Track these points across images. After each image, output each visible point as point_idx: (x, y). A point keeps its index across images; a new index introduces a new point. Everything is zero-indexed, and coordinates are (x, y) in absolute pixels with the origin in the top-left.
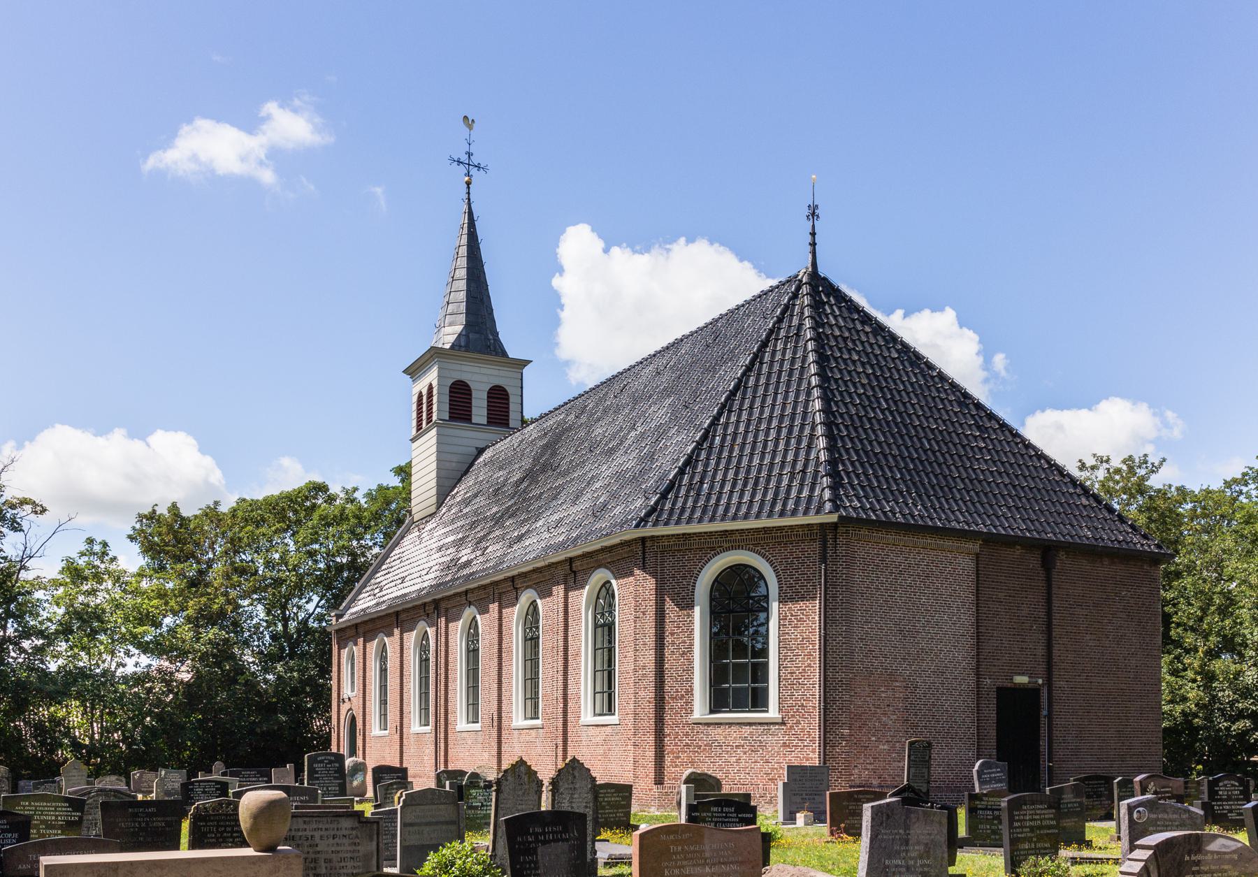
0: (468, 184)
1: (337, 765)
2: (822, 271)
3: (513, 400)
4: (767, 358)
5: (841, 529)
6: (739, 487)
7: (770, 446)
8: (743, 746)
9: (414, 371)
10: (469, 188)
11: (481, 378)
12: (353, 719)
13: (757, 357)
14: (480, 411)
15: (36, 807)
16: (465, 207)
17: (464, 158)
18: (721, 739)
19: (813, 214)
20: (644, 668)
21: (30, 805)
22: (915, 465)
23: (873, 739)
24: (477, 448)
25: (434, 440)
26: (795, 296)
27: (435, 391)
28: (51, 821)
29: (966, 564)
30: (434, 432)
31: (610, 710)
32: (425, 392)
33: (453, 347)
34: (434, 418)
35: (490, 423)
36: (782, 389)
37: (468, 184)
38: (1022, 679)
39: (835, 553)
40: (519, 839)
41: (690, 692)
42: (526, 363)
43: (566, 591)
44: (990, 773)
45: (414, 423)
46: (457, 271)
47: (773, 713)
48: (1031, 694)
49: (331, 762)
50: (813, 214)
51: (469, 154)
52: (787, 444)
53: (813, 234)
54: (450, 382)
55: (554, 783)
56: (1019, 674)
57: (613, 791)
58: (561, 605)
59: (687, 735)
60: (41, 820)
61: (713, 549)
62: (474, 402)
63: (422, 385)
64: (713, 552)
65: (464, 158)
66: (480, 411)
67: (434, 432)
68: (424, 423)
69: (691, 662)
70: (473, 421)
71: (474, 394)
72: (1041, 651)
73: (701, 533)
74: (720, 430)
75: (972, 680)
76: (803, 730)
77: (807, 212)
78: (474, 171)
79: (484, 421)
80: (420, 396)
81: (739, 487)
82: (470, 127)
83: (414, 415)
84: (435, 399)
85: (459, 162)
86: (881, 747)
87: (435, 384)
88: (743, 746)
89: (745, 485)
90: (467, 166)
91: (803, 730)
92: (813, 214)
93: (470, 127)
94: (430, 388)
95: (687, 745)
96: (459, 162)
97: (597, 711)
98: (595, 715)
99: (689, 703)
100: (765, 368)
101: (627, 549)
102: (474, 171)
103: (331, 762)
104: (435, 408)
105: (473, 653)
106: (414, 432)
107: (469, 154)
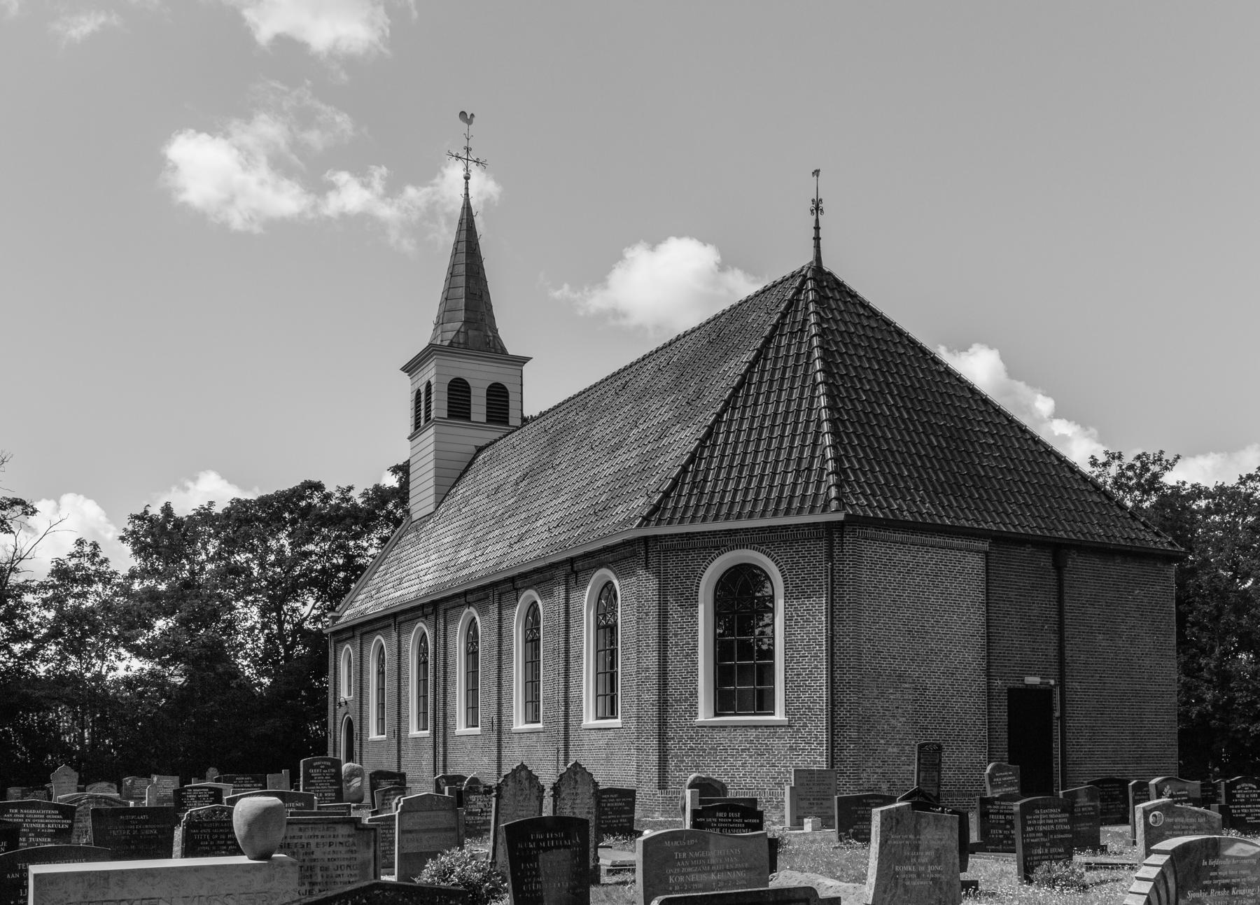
1: (333, 770)
2: (827, 266)
3: (513, 397)
5: (848, 528)
8: (749, 749)
10: (467, 183)
11: (480, 375)
12: (350, 724)
14: (479, 408)
19: (817, 208)
20: (647, 670)
21: (19, 813)
23: (882, 741)
24: (476, 447)
25: (432, 439)
26: (799, 291)
27: (433, 389)
29: (975, 563)
32: (423, 390)
34: (433, 416)
41: (694, 694)
42: (527, 359)
44: (1001, 777)
48: (1043, 695)
49: (327, 767)
50: (817, 209)
53: (817, 228)
56: (1031, 675)
59: (691, 738)
61: (717, 548)
64: (717, 552)
66: (479, 408)
67: (432, 431)
68: (422, 423)
69: (695, 663)
72: (1052, 652)
76: (810, 733)
77: (811, 206)
79: (484, 419)
82: (469, 122)
86: (890, 750)
87: (433, 381)
88: (749, 749)
90: (465, 161)
91: (810, 733)
92: (817, 209)
93: (469, 122)
94: (429, 385)
95: (692, 748)
96: (477, 162)
99: (694, 705)
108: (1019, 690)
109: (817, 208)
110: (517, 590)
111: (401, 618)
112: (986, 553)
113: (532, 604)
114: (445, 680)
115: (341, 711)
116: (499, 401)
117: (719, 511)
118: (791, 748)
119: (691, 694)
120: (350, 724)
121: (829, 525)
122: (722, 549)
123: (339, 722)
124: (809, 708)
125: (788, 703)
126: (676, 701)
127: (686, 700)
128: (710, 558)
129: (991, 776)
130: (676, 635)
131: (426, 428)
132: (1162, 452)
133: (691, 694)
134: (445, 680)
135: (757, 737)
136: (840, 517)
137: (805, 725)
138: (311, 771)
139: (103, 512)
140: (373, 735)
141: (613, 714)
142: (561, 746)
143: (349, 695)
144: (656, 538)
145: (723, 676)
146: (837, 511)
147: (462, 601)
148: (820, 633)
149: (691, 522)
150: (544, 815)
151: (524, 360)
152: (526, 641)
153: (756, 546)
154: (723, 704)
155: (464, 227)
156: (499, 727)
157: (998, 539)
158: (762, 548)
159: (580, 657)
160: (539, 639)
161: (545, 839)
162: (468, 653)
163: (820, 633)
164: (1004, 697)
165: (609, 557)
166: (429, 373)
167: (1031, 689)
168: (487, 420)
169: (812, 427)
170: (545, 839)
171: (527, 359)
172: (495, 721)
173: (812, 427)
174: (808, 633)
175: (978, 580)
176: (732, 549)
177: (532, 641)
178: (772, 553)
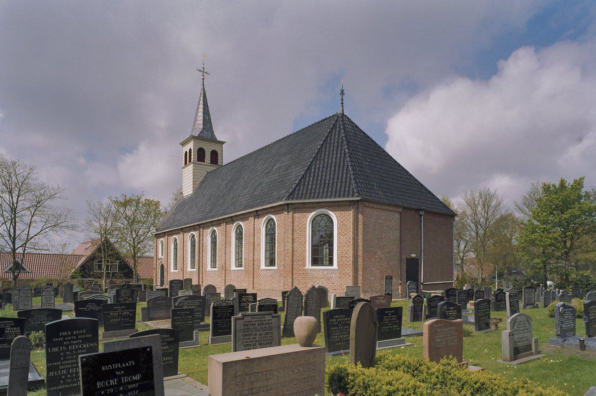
0: (203, 79)
3: (219, 155)
4: (328, 142)
5: (360, 203)
6: (322, 186)
7: (332, 172)
9: (183, 144)
11: (208, 148)
12: (162, 266)
13: (325, 140)
16: (202, 87)
17: (202, 69)
19: (342, 93)
22: (362, 181)
25: (192, 168)
26: (337, 121)
27: (192, 151)
29: (397, 216)
30: (192, 165)
32: (188, 151)
34: (192, 160)
35: (211, 163)
36: (335, 152)
37: (203, 79)
38: (414, 255)
40: (331, 320)
41: (305, 258)
42: (224, 142)
45: (184, 162)
47: (335, 266)
49: (178, 283)
50: (342, 93)
51: (204, 68)
52: (339, 172)
53: (342, 100)
55: (307, 296)
58: (253, 227)
61: (313, 208)
62: (206, 155)
63: (186, 148)
65: (202, 69)
67: (192, 165)
68: (188, 162)
69: (305, 247)
71: (206, 153)
74: (313, 167)
75: (399, 255)
77: (340, 92)
78: (205, 74)
80: (186, 152)
81: (322, 186)
83: (184, 159)
84: (192, 154)
85: (200, 71)
87: (192, 148)
89: (324, 186)
92: (342, 93)
94: (190, 150)
95: (304, 277)
96: (200, 71)
97: (237, 266)
98: (211, 268)
99: (305, 262)
100: (328, 146)
101: (281, 207)
102: (205, 74)
103: (178, 283)
104: (192, 157)
105: (214, 242)
106: (184, 165)
107: (204, 68)
108: (410, 259)
109: (342, 93)
110: (233, 221)
111: (184, 230)
112: (400, 213)
113: (239, 226)
115: (159, 262)
116: (215, 157)
117: (314, 195)
120: (162, 266)
121: (358, 201)
123: (158, 266)
124: (346, 264)
125: (338, 262)
129: (409, 285)
130: (298, 238)
131: (189, 165)
133: (304, 259)
135: (327, 274)
136: (359, 198)
139: (513, 54)
140: (172, 270)
143: (162, 255)
144: (291, 204)
145: (316, 250)
146: (357, 196)
147: (210, 224)
148: (350, 238)
149: (313, 198)
150: (474, 321)
151: (223, 143)
152: (236, 239)
154: (315, 261)
155: (202, 95)
156: (225, 269)
157: (404, 208)
159: (259, 244)
160: (216, 242)
161: (339, 318)
162: (191, 246)
164: (405, 261)
165: (273, 210)
166: (191, 145)
167: (413, 259)
169: (346, 167)
170: (339, 318)
171: (224, 142)
172: (224, 267)
173: (346, 167)
177: (214, 242)
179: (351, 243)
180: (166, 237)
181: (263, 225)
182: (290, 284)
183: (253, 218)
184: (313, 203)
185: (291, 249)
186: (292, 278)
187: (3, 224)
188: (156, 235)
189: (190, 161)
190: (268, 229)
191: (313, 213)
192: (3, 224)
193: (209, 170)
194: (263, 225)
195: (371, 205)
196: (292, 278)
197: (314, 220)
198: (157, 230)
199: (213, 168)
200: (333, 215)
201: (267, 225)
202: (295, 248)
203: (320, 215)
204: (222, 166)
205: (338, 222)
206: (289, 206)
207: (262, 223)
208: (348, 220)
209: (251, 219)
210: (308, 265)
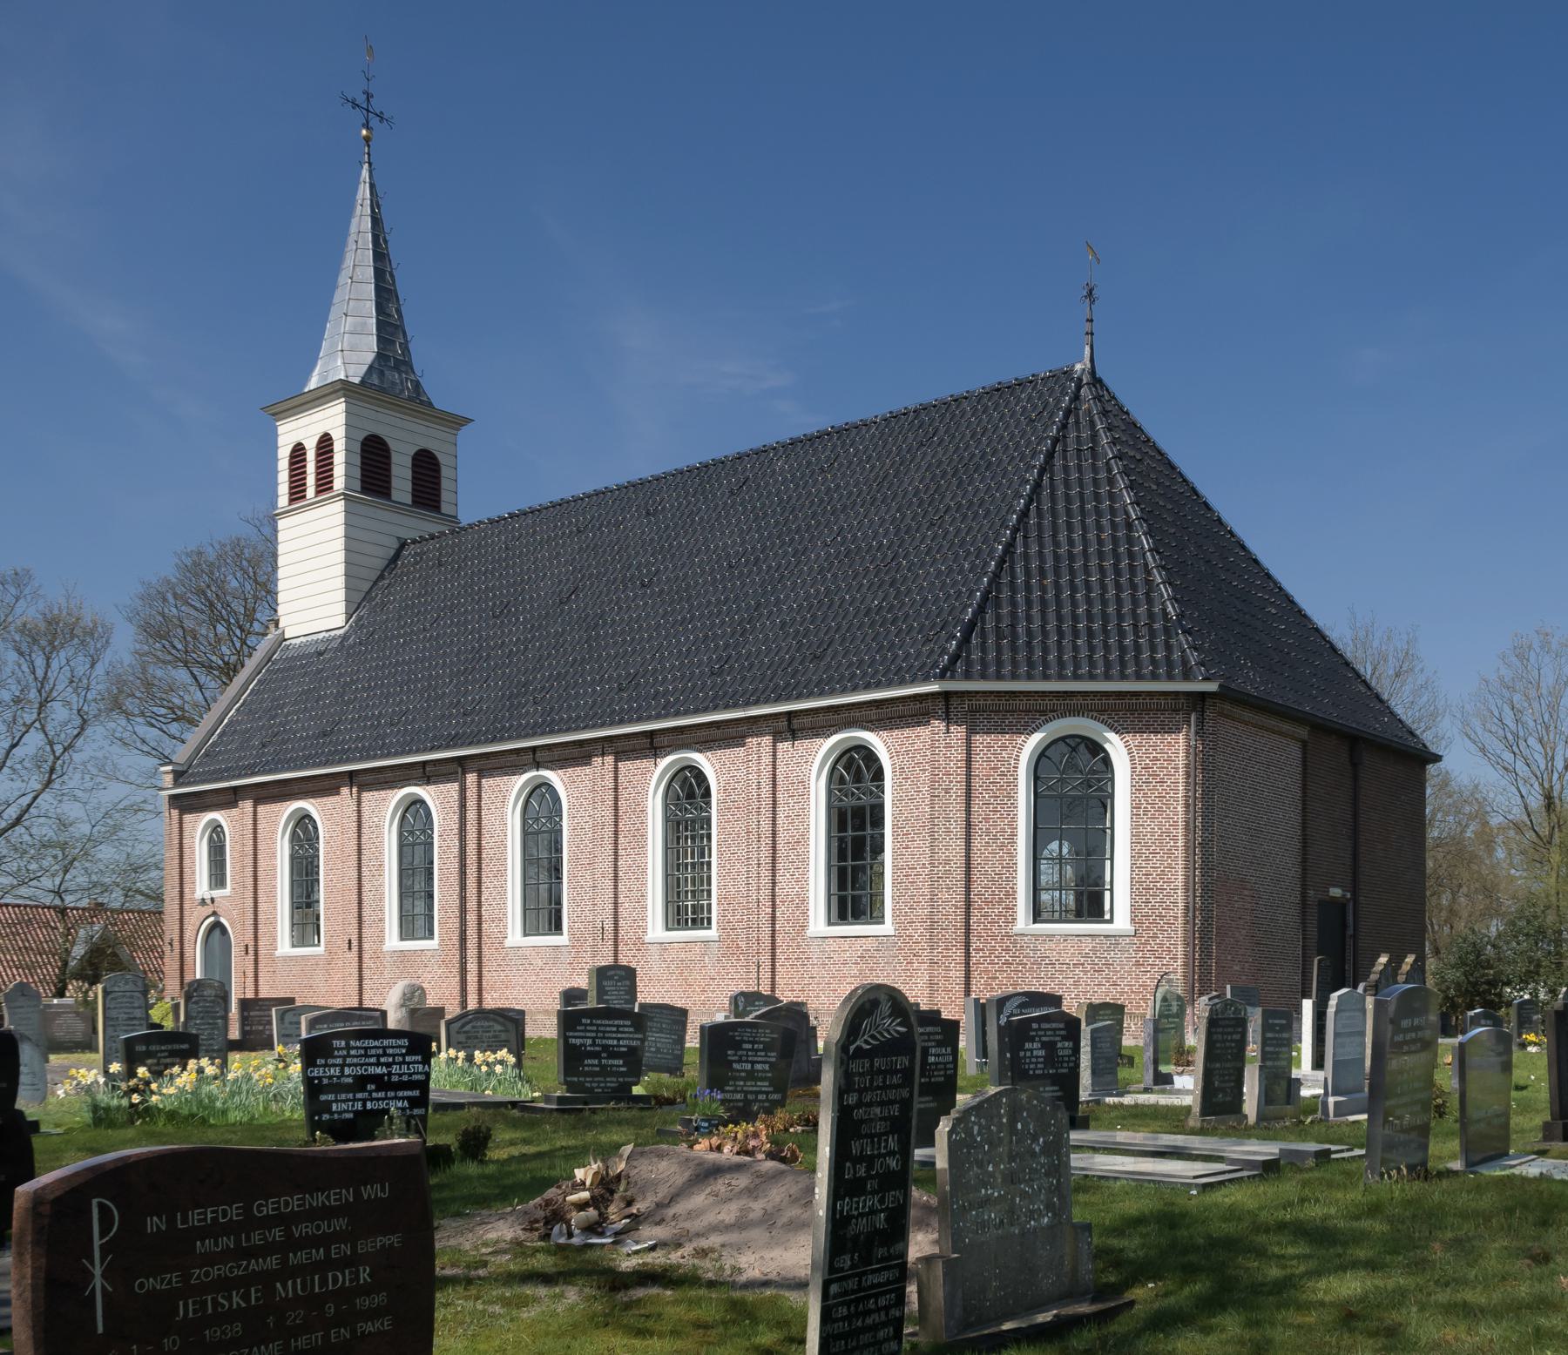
1: (628, 983)
2: (1099, 374)
8: (1083, 964)
11: (405, 438)
15: (598, 1026)
17: (361, 99)
18: (1054, 956)
20: (947, 862)
21: (591, 1024)
23: (1229, 958)
24: (398, 538)
28: (613, 1046)
31: (556, 926)
33: (363, 382)
38: (1336, 892)
39: (1202, 729)
41: (1011, 894)
43: (616, 761)
46: (357, 269)
47: (1122, 921)
48: (1339, 906)
51: (369, 96)
54: (361, 436)
57: (1109, 1012)
59: (1007, 950)
60: (603, 1046)
61: (1043, 713)
62: (408, 474)
64: (1043, 718)
65: (361, 99)
70: (393, 498)
71: (395, 458)
73: (1030, 692)
76: (1161, 945)
79: (408, 499)
85: (355, 105)
88: (1083, 964)
91: (1161, 945)
94: (325, 443)
95: (1007, 963)
99: (1011, 908)
107: (369, 96)
114: (479, 869)
118: (1137, 964)
119: (1007, 895)
121: (1203, 696)
122: (1051, 715)
124: (1161, 917)
126: (987, 903)
127: (1000, 902)
128: (1034, 726)
130: (987, 819)
132: (175, 553)
134: (479, 869)
135: (1094, 949)
136: (1212, 687)
137: (1155, 937)
138: (605, 983)
141: (556, 926)
142: (765, 959)
148: (1175, 825)
153: (1095, 714)
158: (1102, 717)
163: (1175, 825)
168: (413, 501)
174: (1160, 825)
175: (1295, 768)
176: (1064, 715)
178: (1116, 724)
179: (1180, 843)
180: (471, 778)
181: (201, 839)
182: (960, 988)
183: (767, 740)
184: (1043, 694)
185: (961, 862)
186: (967, 964)
187: (1087, 333)
188: (173, 798)
189: (324, 484)
190: (531, 814)
191: (1037, 737)
192: (1087, 333)
193: (408, 535)
194: (201, 839)
195: (1237, 711)
196: (967, 964)
197: (1042, 758)
198: (179, 776)
199: (418, 525)
200: (1116, 746)
201: (403, 817)
202: (976, 859)
203: (1063, 739)
204: (459, 531)
205: (1133, 769)
206: (954, 701)
207: (385, 806)
208: (1169, 760)
209: (247, 805)
210: (1022, 920)
